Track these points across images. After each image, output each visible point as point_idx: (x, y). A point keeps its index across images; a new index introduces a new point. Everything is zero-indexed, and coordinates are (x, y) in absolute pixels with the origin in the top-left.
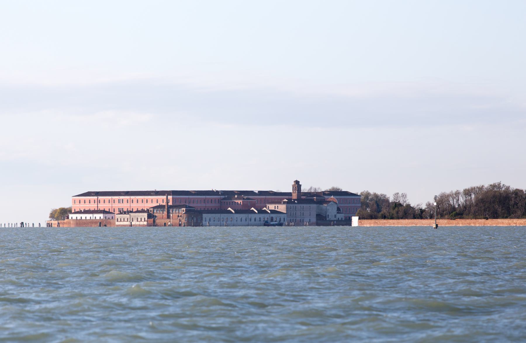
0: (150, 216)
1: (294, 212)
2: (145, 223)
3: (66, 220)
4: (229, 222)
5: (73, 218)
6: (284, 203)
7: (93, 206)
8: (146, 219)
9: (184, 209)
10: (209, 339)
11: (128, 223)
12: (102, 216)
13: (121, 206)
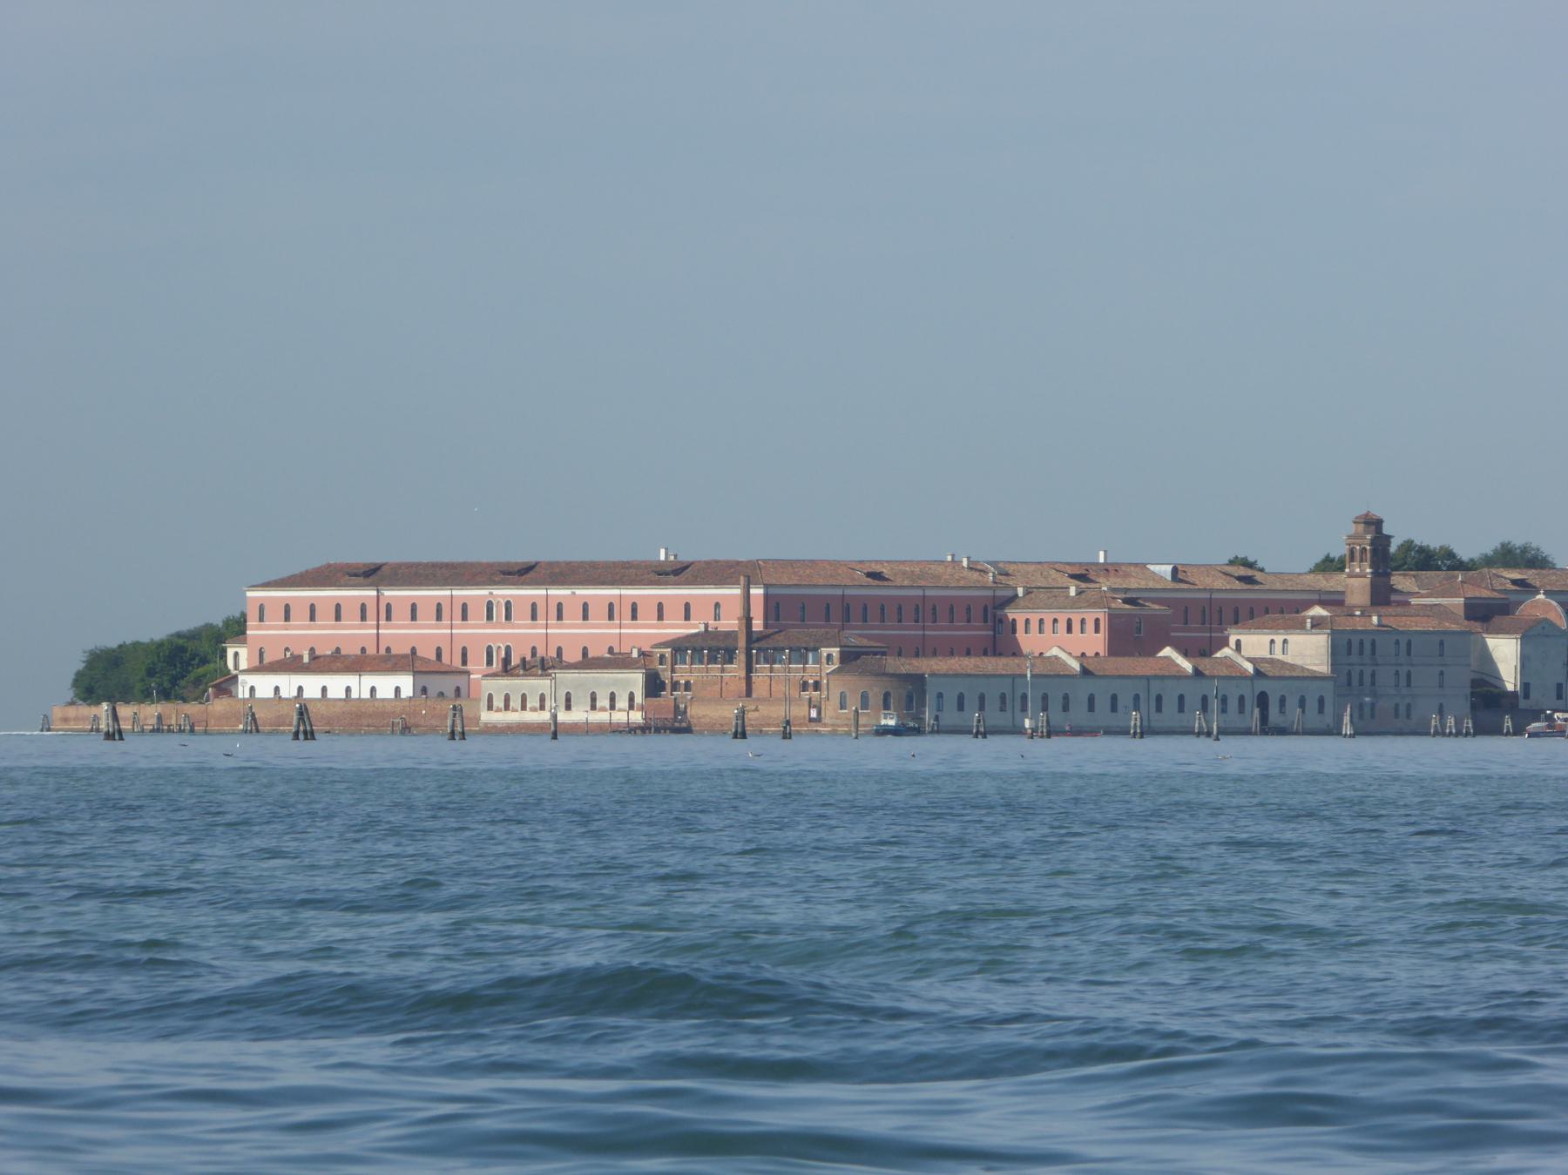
0: (654, 686)
1: (1368, 671)
2: (637, 717)
3: (219, 706)
4: (1103, 715)
5: (284, 694)
6: (1318, 624)
7: (355, 634)
8: (639, 699)
9: (835, 651)
10: (315, 1113)
11: (545, 716)
13: (499, 634)
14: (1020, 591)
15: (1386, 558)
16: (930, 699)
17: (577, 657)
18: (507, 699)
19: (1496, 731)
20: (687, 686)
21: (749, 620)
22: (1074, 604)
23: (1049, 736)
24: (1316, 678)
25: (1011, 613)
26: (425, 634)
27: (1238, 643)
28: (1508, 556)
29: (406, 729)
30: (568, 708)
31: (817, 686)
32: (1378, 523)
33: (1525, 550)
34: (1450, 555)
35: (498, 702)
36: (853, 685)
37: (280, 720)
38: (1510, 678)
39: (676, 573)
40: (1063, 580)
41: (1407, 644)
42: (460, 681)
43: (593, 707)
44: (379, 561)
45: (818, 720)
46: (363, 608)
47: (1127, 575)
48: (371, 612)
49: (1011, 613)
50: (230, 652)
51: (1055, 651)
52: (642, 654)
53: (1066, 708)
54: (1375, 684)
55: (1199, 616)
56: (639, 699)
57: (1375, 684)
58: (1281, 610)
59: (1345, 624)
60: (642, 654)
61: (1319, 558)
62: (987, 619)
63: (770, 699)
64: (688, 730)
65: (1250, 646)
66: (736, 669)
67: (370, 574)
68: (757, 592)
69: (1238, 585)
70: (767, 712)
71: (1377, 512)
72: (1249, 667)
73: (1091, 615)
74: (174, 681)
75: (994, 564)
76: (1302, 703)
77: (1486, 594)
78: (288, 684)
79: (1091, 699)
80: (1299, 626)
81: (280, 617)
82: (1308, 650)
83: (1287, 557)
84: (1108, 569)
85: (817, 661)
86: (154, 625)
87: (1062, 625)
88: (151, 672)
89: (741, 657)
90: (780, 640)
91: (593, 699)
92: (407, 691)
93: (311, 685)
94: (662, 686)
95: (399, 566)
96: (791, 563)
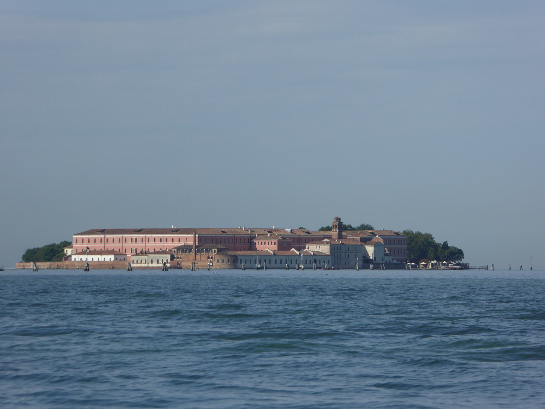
0: (172, 258)
3: (67, 263)
4: (273, 264)
5: (77, 260)
6: (327, 243)
7: (99, 246)
8: (169, 261)
12: (112, 257)
13: (134, 245)
14: (256, 235)
15: (342, 227)
16: (239, 261)
17: (153, 251)
18: (137, 261)
19: (368, 268)
20: (181, 258)
21: (195, 242)
22: (269, 238)
23: (245, 269)
24: (327, 256)
25: (255, 241)
26: (116, 246)
27: (308, 248)
28: (364, 227)
29: (113, 268)
30: (152, 263)
31: (212, 258)
32: (340, 219)
33: (367, 226)
34: (351, 227)
35: (135, 262)
36: (221, 257)
37: (83, 266)
38: (371, 256)
39: (177, 231)
40: (266, 233)
41: (347, 248)
42: (123, 257)
43: (158, 263)
44: (104, 228)
45: (212, 265)
46: (101, 239)
47: (280, 232)
48: (103, 240)
49: (255, 241)
50: (65, 250)
51: (267, 249)
52: (169, 250)
53: (270, 263)
54: (340, 258)
55: (300, 240)
56: (169, 261)
57: (340, 258)
58: (318, 240)
59: (334, 243)
60: (169, 250)
61: (320, 228)
62: (249, 242)
63: (200, 261)
64: (181, 268)
65: (311, 248)
66: (192, 254)
67: (103, 232)
68: (197, 235)
69: (306, 234)
70: (198, 264)
71: (339, 217)
72: (312, 253)
73: (273, 241)
74: (52, 257)
75: (250, 229)
76: (324, 261)
77: (365, 236)
78: (84, 258)
79: (276, 260)
80: (323, 243)
81: (80, 241)
82: (325, 249)
83: (313, 227)
84: (276, 230)
85: (212, 252)
86: (41, 243)
87: (267, 243)
88: (46, 255)
89: (193, 251)
90: (203, 247)
91: (158, 261)
92: (113, 259)
93: (90, 258)
94: (174, 258)
95: (110, 230)
96: (203, 229)
